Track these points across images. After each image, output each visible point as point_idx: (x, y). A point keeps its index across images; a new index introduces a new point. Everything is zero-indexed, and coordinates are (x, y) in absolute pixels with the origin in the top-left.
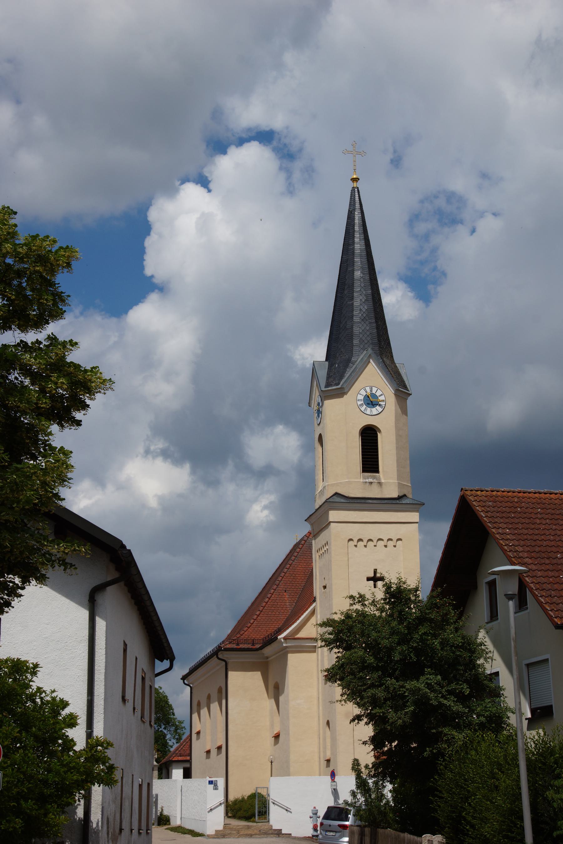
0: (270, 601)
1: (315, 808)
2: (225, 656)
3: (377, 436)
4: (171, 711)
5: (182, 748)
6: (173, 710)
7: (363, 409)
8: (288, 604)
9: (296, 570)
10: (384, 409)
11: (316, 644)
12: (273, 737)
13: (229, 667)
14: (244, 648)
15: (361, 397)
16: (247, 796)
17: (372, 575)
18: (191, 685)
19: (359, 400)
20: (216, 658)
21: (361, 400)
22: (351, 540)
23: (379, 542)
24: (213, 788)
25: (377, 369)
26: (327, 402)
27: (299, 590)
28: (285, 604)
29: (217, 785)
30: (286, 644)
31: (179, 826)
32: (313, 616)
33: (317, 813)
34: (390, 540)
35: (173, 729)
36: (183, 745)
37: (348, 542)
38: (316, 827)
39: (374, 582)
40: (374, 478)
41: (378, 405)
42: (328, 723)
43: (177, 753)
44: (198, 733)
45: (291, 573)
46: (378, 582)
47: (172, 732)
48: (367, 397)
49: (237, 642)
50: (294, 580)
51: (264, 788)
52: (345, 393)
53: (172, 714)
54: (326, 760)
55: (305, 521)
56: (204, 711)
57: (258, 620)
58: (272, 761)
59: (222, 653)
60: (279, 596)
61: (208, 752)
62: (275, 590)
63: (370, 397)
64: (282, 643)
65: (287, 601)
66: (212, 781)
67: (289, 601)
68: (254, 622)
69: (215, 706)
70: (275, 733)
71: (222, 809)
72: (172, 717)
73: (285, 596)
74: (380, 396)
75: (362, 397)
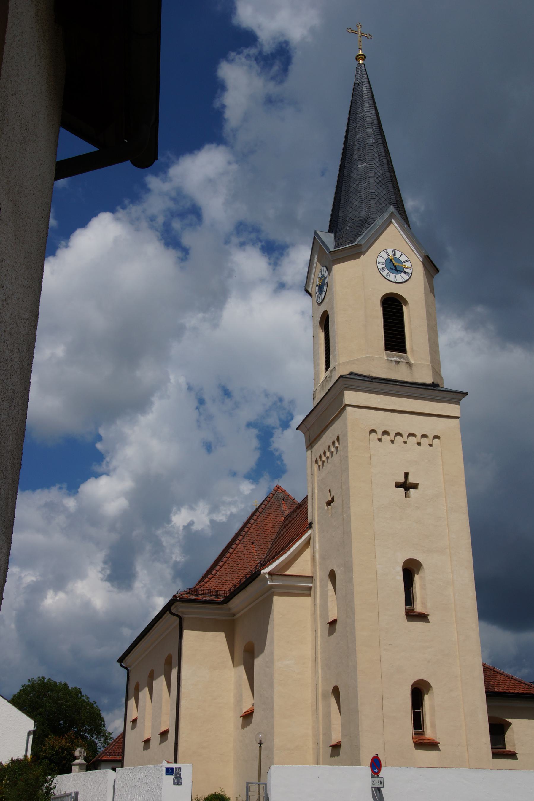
0: (235, 552)
2: (181, 610)
3: (402, 309)
4: (103, 723)
5: (112, 748)
7: (385, 273)
8: (257, 557)
9: (264, 523)
10: (411, 277)
11: (311, 585)
12: (240, 717)
13: (185, 624)
14: (205, 600)
15: (381, 260)
16: (204, 798)
17: (402, 480)
18: (129, 669)
19: (379, 263)
20: (170, 614)
21: (382, 263)
22: (373, 431)
23: (410, 438)
24: (174, 781)
25: (400, 231)
26: (337, 268)
27: (268, 543)
28: (254, 556)
29: (180, 777)
30: (272, 582)
32: (307, 547)
34: (424, 436)
35: (103, 739)
36: (113, 745)
37: (370, 434)
39: (405, 490)
40: (401, 357)
41: (403, 272)
42: (336, 691)
44: (135, 721)
45: (259, 525)
46: (411, 490)
47: (102, 741)
48: (389, 261)
49: (197, 593)
50: (262, 532)
52: (363, 253)
54: (330, 746)
55: (297, 429)
56: (144, 693)
57: (221, 572)
58: (260, 741)
60: (246, 548)
61: (147, 742)
62: (241, 541)
63: (393, 261)
64: (266, 580)
65: (256, 554)
66: (172, 769)
67: (258, 554)
68: (216, 573)
69: (160, 683)
72: (103, 728)
73: (253, 549)
74: (405, 262)
75: (383, 261)
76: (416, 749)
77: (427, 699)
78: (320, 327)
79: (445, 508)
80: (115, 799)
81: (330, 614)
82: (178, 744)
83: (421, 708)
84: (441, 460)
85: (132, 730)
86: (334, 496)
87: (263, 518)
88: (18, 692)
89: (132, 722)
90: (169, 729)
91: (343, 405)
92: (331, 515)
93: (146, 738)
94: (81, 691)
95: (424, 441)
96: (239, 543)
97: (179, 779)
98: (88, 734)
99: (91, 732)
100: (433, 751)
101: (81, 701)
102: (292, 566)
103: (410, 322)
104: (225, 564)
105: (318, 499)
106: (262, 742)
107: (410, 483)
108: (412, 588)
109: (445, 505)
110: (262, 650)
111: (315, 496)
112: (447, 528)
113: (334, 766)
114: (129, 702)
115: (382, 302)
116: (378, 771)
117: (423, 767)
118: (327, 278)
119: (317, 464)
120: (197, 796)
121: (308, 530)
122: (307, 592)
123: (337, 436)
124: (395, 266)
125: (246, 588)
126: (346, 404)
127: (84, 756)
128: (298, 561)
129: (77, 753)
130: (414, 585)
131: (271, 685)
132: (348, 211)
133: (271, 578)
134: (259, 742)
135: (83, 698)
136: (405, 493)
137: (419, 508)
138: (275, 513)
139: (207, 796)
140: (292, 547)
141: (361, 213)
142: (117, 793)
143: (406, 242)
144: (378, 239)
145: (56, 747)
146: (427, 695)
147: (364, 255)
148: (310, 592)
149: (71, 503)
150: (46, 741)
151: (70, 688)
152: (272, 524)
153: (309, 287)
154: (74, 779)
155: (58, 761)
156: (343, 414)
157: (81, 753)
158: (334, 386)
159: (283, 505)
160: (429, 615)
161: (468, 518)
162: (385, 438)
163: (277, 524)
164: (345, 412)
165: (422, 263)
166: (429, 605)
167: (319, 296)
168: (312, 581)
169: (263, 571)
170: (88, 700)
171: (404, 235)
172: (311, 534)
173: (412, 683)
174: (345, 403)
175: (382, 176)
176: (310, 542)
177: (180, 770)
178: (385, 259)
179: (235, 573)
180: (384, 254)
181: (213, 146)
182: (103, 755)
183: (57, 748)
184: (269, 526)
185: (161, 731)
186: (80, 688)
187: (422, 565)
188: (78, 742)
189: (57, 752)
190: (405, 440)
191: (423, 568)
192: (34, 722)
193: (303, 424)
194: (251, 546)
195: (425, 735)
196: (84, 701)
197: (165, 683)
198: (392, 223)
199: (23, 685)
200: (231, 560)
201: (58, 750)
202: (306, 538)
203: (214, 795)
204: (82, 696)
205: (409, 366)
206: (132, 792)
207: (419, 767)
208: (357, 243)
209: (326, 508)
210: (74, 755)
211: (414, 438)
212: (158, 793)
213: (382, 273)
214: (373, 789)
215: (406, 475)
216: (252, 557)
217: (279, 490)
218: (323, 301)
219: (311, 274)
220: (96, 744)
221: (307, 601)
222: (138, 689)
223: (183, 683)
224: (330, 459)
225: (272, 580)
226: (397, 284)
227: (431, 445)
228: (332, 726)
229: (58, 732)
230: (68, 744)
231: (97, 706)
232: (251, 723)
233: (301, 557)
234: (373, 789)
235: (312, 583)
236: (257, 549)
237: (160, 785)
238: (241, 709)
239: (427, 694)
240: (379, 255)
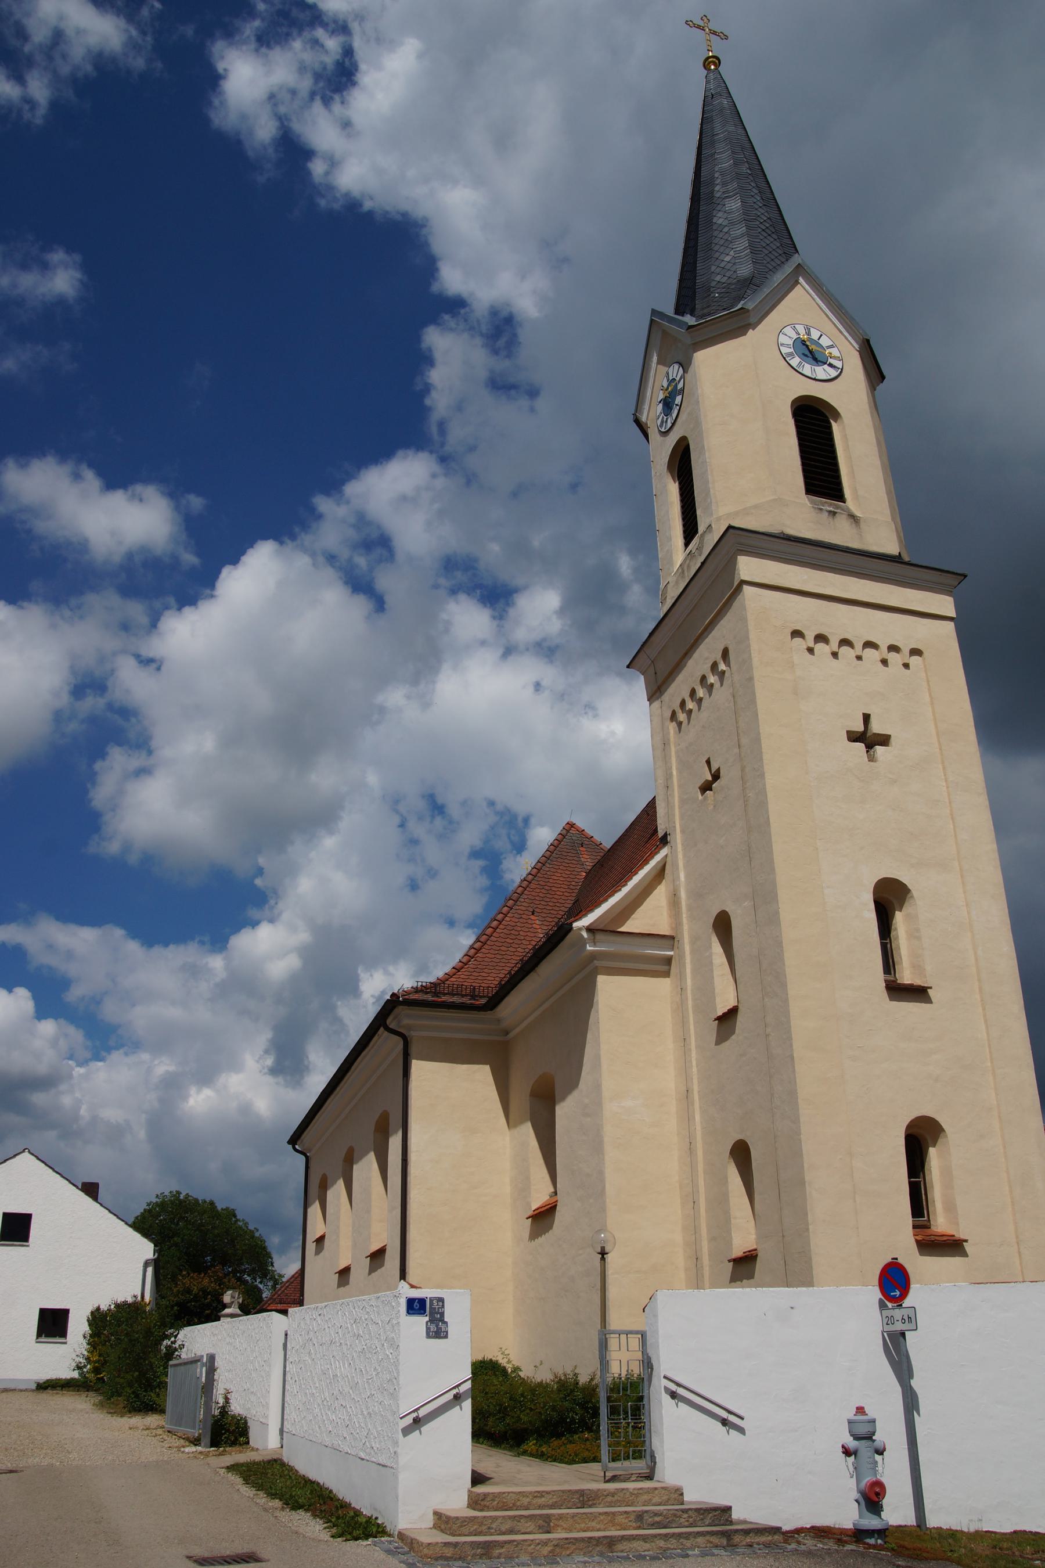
0: (501, 926)
1: (860, 1410)
4: (270, 1260)
5: (284, 1291)
6: (272, 1259)
9: (551, 881)
11: (671, 953)
13: (414, 1049)
14: (453, 1002)
19: (782, 345)
21: (788, 346)
22: (797, 634)
23: (867, 650)
24: (428, 1329)
25: (816, 297)
26: (703, 358)
30: (595, 945)
31: (275, 1460)
32: (660, 883)
33: (874, 1433)
35: (270, 1284)
38: (877, 1494)
40: (838, 507)
41: (825, 363)
43: (275, 1299)
44: (320, 1240)
46: (877, 747)
47: (270, 1287)
51: (628, 1333)
52: (754, 326)
53: (270, 1264)
54: (729, 1261)
55: (628, 667)
56: (337, 1192)
57: (478, 959)
58: (603, 1248)
59: (394, 1019)
61: (344, 1273)
64: (583, 942)
65: (539, 931)
66: (422, 1301)
68: (470, 961)
69: (366, 1168)
70: (534, 1208)
71: (462, 1416)
72: (270, 1268)
74: (829, 347)
76: (921, 1255)
77: (934, 1156)
78: (669, 474)
79: (944, 784)
80: (287, 1369)
81: (718, 1000)
82: (407, 1271)
83: (922, 1175)
84: (927, 694)
85: (316, 1256)
86: (719, 768)
87: (548, 873)
88: (141, 1213)
89: (315, 1243)
90: (386, 1245)
91: (736, 584)
92: (714, 806)
93: (342, 1266)
94: (235, 1214)
95: (892, 657)
96: (509, 912)
97: (440, 1324)
98: (249, 1275)
99: (252, 1272)
100: (955, 1257)
101: (236, 1227)
102: (632, 917)
103: (847, 448)
104: (484, 947)
105: (680, 786)
106: (607, 1250)
107: (875, 734)
108: (888, 939)
109: (943, 777)
110: (573, 1083)
111: (672, 782)
112: (951, 822)
113: (799, 1289)
114: (310, 1210)
115: (793, 409)
116: (900, 1296)
117: (987, 1283)
118: (683, 379)
119: (674, 723)
121: (661, 848)
122: (663, 967)
123: (722, 648)
124: (811, 352)
125: (536, 969)
126: (741, 580)
127: (238, 1302)
128: (642, 908)
129: (227, 1298)
130: (893, 934)
131: (597, 1147)
132: (713, 272)
133: (593, 937)
134: (599, 1250)
135: (239, 1223)
136: (867, 752)
137: (895, 782)
138: (570, 865)
140: (632, 878)
141: (738, 272)
142: (291, 1358)
143: (827, 316)
144: (777, 305)
145: (194, 1289)
146: (934, 1148)
147: (753, 330)
149: (216, 963)
150: (179, 1279)
151: (219, 1208)
152: (574, 859)
153: (641, 413)
154: (212, 1333)
155: (198, 1310)
156: (736, 604)
158: (714, 552)
159: (583, 853)
160: (930, 988)
161: (987, 803)
162: (820, 647)
163: (573, 883)
164: (739, 597)
165: (858, 353)
166: (928, 968)
167: (665, 420)
168: (673, 945)
169: (576, 925)
170: (247, 1227)
171: (823, 305)
172: (666, 856)
173: (907, 1123)
174: (740, 578)
175: (769, 221)
176: (664, 872)
177: (440, 1304)
178: (793, 340)
179: (503, 960)
180: (788, 331)
181: (410, 453)
182: (269, 1302)
183: (195, 1290)
184: (559, 886)
185: (371, 1252)
186: (235, 1208)
187: (909, 891)
188: (229, 1282)
189: (196, 1296)
190: (859, 654)
191: (912, 897)
192: (153, 1245)
193: (642, 651)
194: (530, 917)
195: (932, 1227)
196: (241, 1227)
197: (375, 1166)
198: (799, 283)
199: (149, 1202)
200: (495, 939)
201: (198, 1293)
202: (658, 863)
204: (237, 1220)
205: (854, 522)
206: (324, 1355)
207: (978, 1283)
208: (741, 307)
209: (700, 797)
210: (223, 1301)
211: (875, 651)
212: (388, 1356)
213: (790, 362)
214: (885, 1334)
215: (867, 718)
216: (532, 935)
217: (572, 829)
218: (673, 424)
219: (646, 388)
220: (260, 1291)
221: (663, 986)
222: (324, 1186)
223: (413, 1157)
224: (704, 704)
225: (595, 944)
226: (817, 382)
227: (906, 666)
228: (733, 1221)
229: (198, 1267)
230: (212, 1285)
231: (260, 1235)
233: (648, 899)
234: (885, 1334)
235: (672, 949)
236: (540, 923)
237: (393, 1339)
238: (529, 1204)
239: (934, 1146)
240: (781, 331)
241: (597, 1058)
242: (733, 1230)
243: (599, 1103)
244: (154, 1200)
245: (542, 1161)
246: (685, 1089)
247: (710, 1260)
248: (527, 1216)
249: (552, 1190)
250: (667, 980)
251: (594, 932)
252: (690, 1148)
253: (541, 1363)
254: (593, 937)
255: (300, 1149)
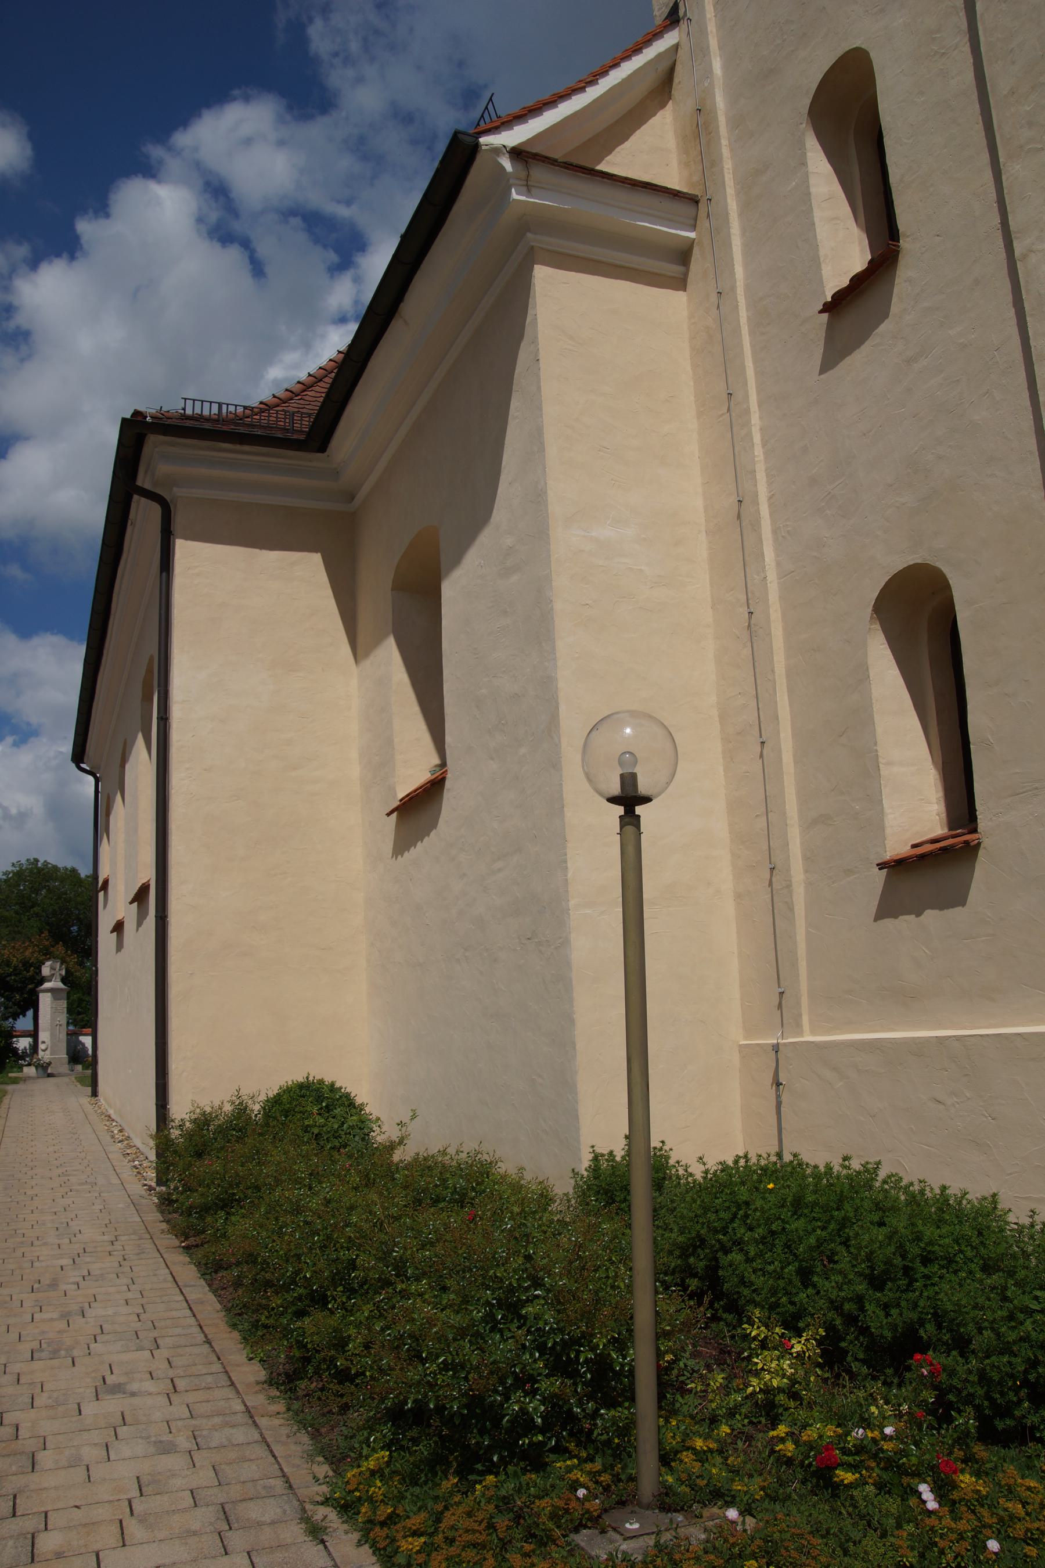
11: (692, 235)
13: (179, 521)
16: (263, 1097)
30: (529, 191)
32: (663, 106)
54: (882, 866)
58: (629, 780)
81: (826, 271)
106: (643, 787)
120: (238, 1091)
127: (60, 975)
128: (627, 144)
129: (46, 970)
139: (276, 1092)
148: (682, 269)
151: (83, 876)
157: (55, 969)
202: (660, 56)
203: (301, 1086)
228: (884, 771)
232: (434, 825)
235: (693, 227)
238: (392, 789)
241: (537, 437)
242: (885, 791)
243: (541, 533)
244: (10, 869)
245: (416, 709)
246: (734, 499)
247: (806, 871)
248: (388, 810)
249: (436, 761)
250: (678, 299)
251: (527, 162)
252: (749, 626)
253: (414, 1117)
254: (525, 173)
255: (88, 768)
